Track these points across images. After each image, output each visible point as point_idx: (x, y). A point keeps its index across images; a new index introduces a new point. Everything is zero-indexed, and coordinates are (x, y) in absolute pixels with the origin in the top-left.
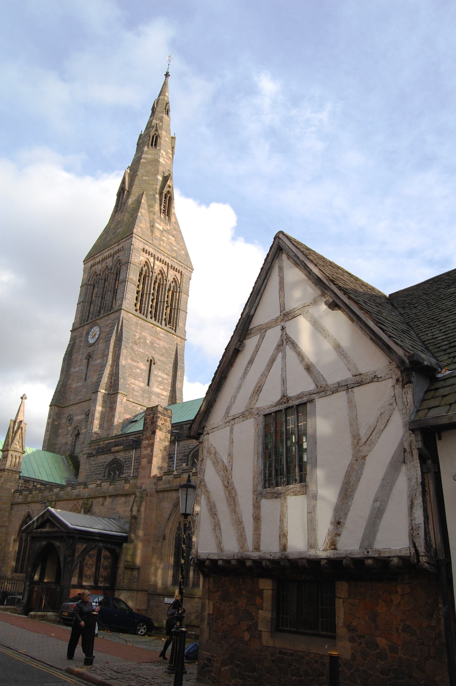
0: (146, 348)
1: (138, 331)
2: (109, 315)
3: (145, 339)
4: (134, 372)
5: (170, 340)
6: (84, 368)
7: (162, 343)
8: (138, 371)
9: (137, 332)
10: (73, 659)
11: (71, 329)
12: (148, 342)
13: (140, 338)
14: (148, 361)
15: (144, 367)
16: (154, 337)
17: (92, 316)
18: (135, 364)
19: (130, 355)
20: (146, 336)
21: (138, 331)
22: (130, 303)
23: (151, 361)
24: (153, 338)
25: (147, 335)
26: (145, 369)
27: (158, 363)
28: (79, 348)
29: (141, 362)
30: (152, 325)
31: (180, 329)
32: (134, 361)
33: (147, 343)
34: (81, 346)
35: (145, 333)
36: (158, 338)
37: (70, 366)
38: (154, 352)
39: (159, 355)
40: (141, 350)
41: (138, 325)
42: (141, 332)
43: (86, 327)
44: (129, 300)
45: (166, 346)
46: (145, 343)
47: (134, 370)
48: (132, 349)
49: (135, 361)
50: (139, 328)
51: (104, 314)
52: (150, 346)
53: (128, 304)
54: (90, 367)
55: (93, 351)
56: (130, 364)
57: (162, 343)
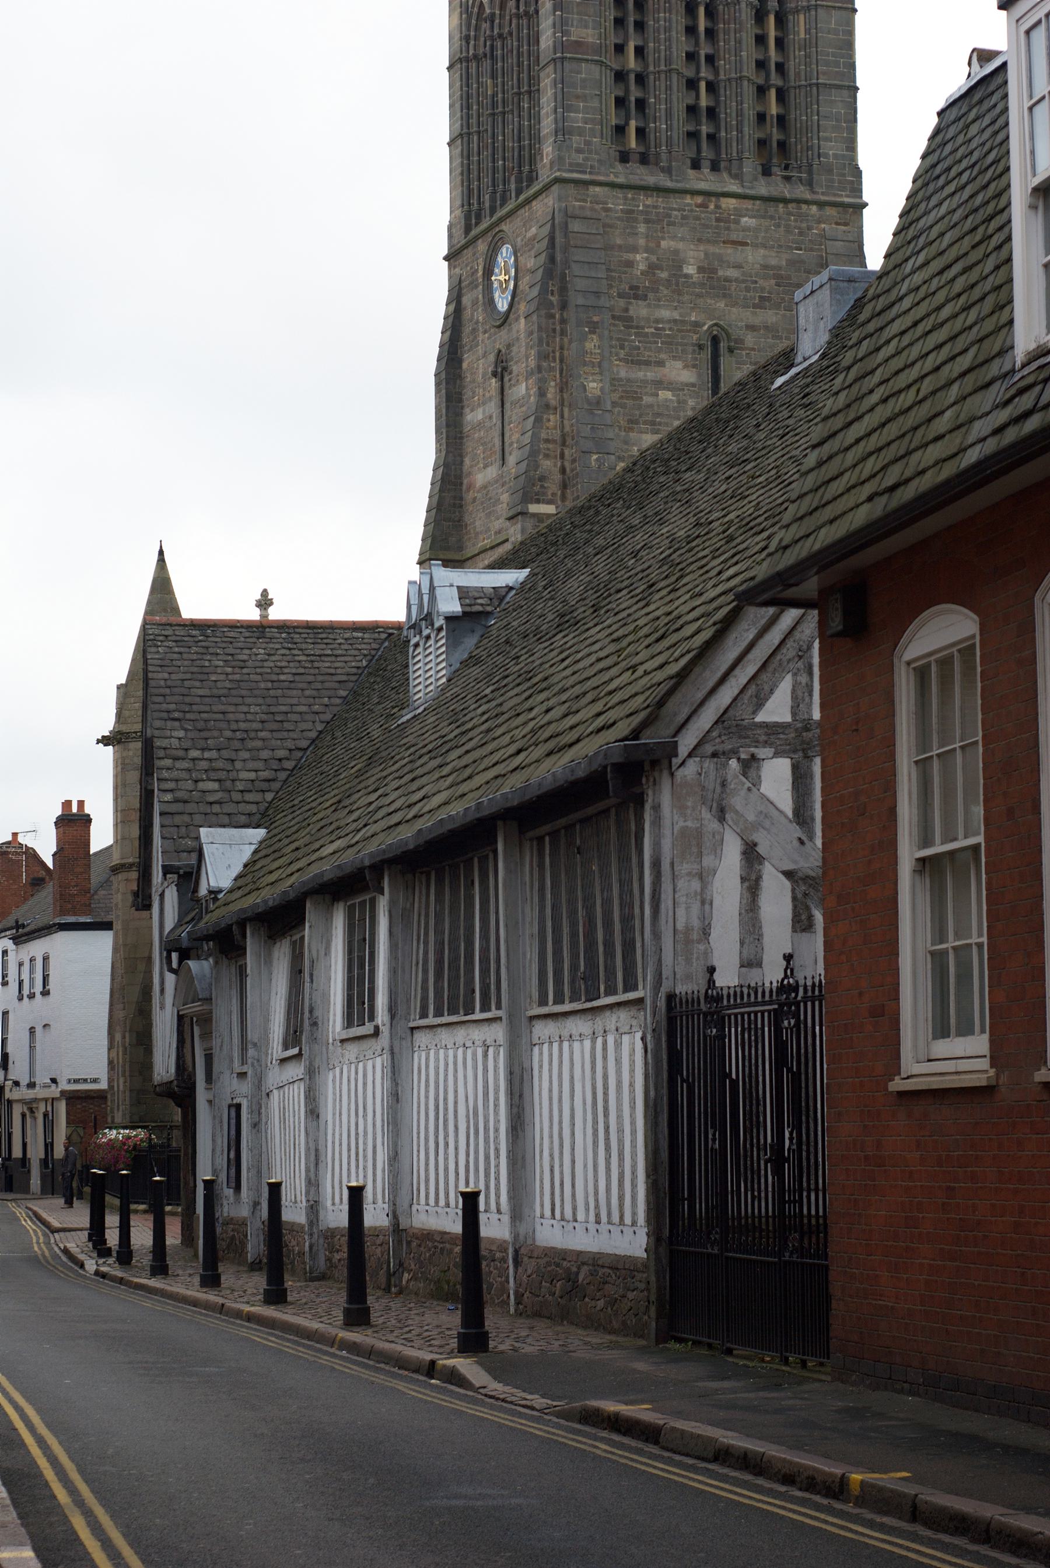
0: (686, 298)
1: (642, 242)
2: (528, 201)
3: (676, 263)
4: (651, 406)
5: (788, 231)
6: (493, 408)
7: (753, 257)
8: (665, 395)
9: (634, 249)
10: (285, 1301)
11: (445, 252)
12: (690, 270)
13: (652, 268)
14: (701, 347)
15: (687, 376)
16: (715, 242)
17: (493, 200)
18: (650, 374)
19: (622, 347)
20: (676, 252)
21: (642, 242)
22: (588, 143)
23: (715, 340)
24: (712, 249)
25: (681, 245)
26: (693, 380)
27: (750, 339)
28: (474, 329)
29: (674, 358)
30: (699, 200)
31: (830, 171)
32: (639, 363)
33: (687, 276)
34: (477, 322)
35: (673, 238)
36: (735, 243)
37: (460, 400)
38: (721, 305)
39: (746, 307)
40: (665, 314)
41: (636, 220)
42: (652, 245)
43: (482, 246)
44: (581, 132)
45: (773, 262)
46: (678, 282)
47: (647, 400)
48: (627, 321)
49: (647, 363)
50: (642, 228)
51: (519, 192)
52: (702, 285)
53: (579, 151)
54: (507, 406)
55: (509, 346)
56: (629, 380)
57: (753, 257)
